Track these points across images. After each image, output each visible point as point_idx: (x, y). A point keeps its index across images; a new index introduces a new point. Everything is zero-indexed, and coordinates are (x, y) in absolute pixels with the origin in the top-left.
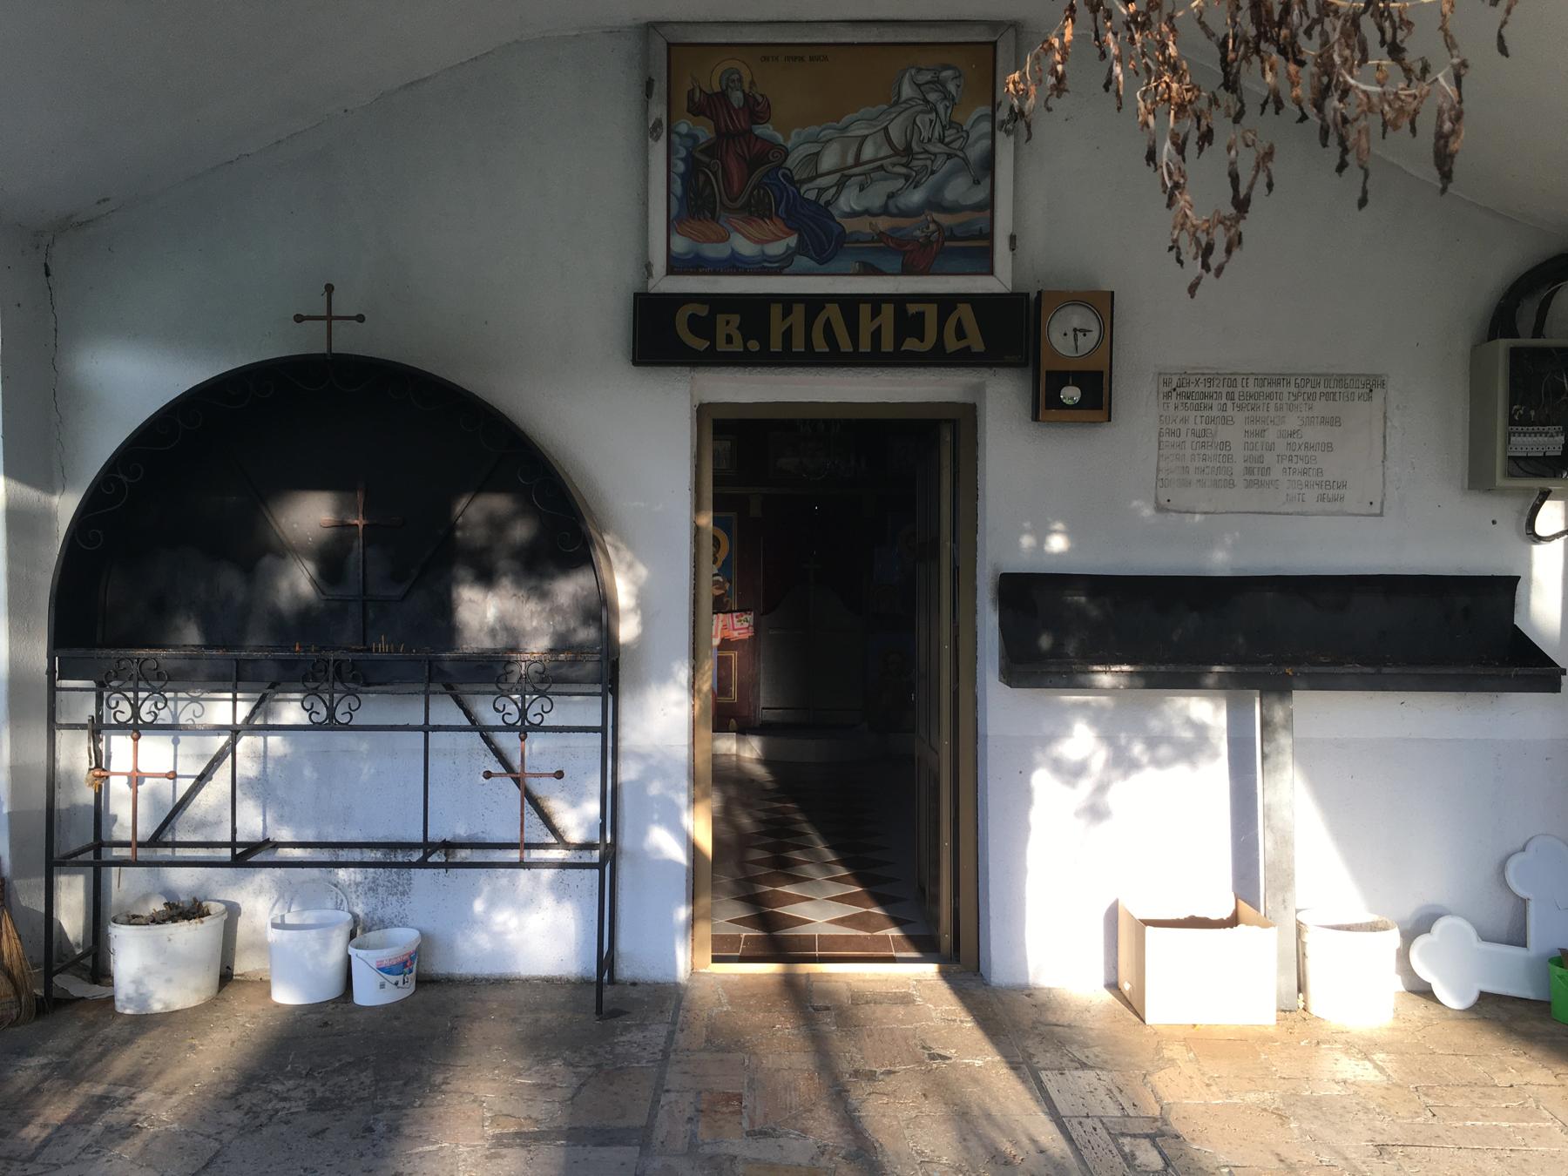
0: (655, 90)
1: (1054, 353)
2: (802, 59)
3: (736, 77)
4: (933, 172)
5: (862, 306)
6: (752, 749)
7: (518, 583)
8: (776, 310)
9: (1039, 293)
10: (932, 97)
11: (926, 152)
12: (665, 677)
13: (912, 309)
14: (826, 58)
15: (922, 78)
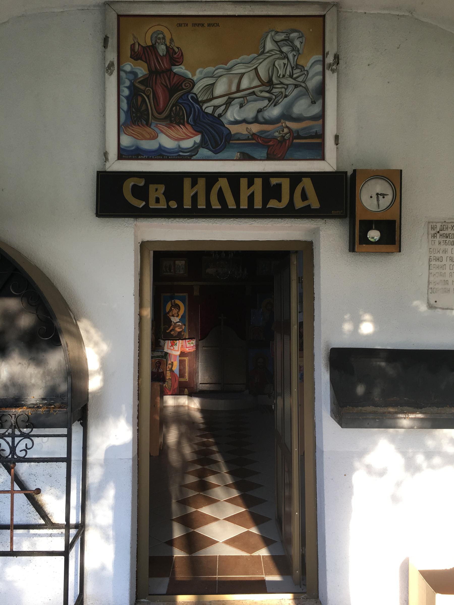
0: (110, 44)
1: (366, 210)
2: (203, 25)
3: (161, 36)
4: (286, 96)
5: (241, 179)
6: (195, 404)
7: (22, 354)
8: (187, 182)
9: (355, 171)
10: (285, 49)
11: (282, 83)
12: (117, 415)
13: (274, 181)
14: (218, 25)
15: (279, 37)
